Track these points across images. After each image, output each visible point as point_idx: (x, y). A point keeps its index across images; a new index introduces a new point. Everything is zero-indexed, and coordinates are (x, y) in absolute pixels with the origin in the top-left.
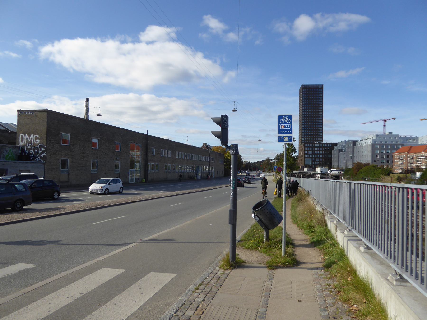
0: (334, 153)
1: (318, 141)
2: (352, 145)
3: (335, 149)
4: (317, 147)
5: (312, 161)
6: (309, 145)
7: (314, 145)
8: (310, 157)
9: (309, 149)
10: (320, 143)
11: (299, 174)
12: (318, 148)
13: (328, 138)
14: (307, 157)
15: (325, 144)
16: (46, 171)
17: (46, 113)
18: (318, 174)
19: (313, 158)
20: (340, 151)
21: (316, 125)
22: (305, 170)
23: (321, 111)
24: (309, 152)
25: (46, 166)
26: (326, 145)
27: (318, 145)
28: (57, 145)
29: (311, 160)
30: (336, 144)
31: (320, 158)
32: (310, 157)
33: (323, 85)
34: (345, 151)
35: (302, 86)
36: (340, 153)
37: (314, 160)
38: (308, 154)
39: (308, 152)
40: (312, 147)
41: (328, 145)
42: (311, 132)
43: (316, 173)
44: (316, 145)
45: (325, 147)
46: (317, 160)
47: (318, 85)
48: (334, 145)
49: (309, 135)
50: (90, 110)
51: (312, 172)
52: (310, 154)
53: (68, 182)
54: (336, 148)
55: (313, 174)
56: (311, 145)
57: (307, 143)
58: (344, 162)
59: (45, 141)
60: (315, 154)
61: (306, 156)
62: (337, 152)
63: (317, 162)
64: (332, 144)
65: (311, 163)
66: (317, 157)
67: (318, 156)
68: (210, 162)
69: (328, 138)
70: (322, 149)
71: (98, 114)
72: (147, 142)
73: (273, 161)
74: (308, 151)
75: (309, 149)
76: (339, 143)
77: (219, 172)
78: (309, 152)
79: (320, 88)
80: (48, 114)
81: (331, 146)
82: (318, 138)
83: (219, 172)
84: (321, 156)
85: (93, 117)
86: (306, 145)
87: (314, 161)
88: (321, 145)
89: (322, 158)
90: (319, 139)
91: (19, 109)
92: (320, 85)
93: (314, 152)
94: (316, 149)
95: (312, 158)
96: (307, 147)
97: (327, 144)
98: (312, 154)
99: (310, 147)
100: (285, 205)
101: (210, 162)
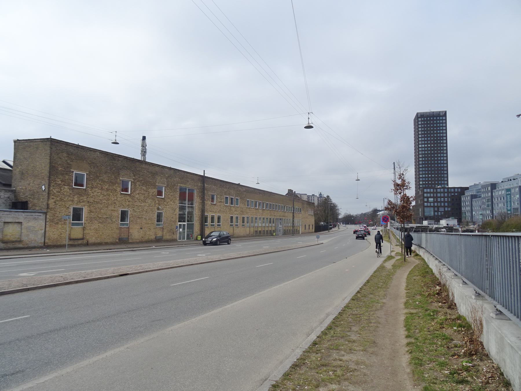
0: (465, 199)
1: (441, 184)
2: (489, 188)
3: (466, 194)
4: (440, 193)
5: (434, 211)
6: (429, 190)
7: (436, 190)
8: (431, 206)
9: (429, 195)
10: (444, 188)
11: (416, 228)
12: (442, 199)
13: (454, 181)
14: (427, 206)
15: (451, 188)
16: (47, 223)
17: (49, 143)
18: (443, 228)
19: (436, 207)
20: (473, 197)
21: (438, 160)
22: (425, 223)
23: (446, 176)
24: (430, 199)
25: (48, 217)
26: (452, 190)
27: (442, 190)
28: (66, 187)
29: (432, 209)
30: (467, 188)
31: (444, 207)
32: (431, 206)
33: (446, 112)
34: (480, 197)
35: (417, 114)
36: (473, 200)
37: (436, 209)
38: (428, 202)
39: (428, 200)
40: (433, 193)
41: (456, 190)
42: (431, 174)
43: (440, 226)
44: (439, 190)
45: (451, 192)
46: (442, 209)
47: (440, 112)
48: (463, 190)
49: (428, 177)
50: (148, 151)
51: (437, 226)
52: (431, 203)
53: (83, 239)
54: (468, 193)
55: (436, 228)
56: (432, 190)
57: (427, 188)
58: (479, 213)
59: (47, 181)
60: (437, 202)
61: (426, 204)
62: (469, 198)
63: (441, 212)
64: (461, 188)
65: (432, 214)
66: (441, 206)
67: (443, 204)
68: (293, 213)
69: (454, 181)
70: (448, 195)
71: (114, 141)
72: (204, 186)
73: (381, 213)
74: (428, 198)
75: (429, 195)
76: (470, 186)
77: (307, 227)
78: (430, 199)
79: (442, 116)
80: (52, 144)
81: (459, 190)
82: (441, 180)
83: (307, 227)
84: (446, 204)
85: (149, 159)
86: (425, 190)
87: (436, 211)
88: (446, 190)
89: (448, 197)
90: (443, 182)
91: (16, 139)
92: (442, 112)
93: (437, 200)
94: (439, 195)
95: (434, 207)
96: (427, 193)
97: (454, 188)
98: (434, 202)
99: (430, 193)
100: (481, 235)
101: (293, 213)
